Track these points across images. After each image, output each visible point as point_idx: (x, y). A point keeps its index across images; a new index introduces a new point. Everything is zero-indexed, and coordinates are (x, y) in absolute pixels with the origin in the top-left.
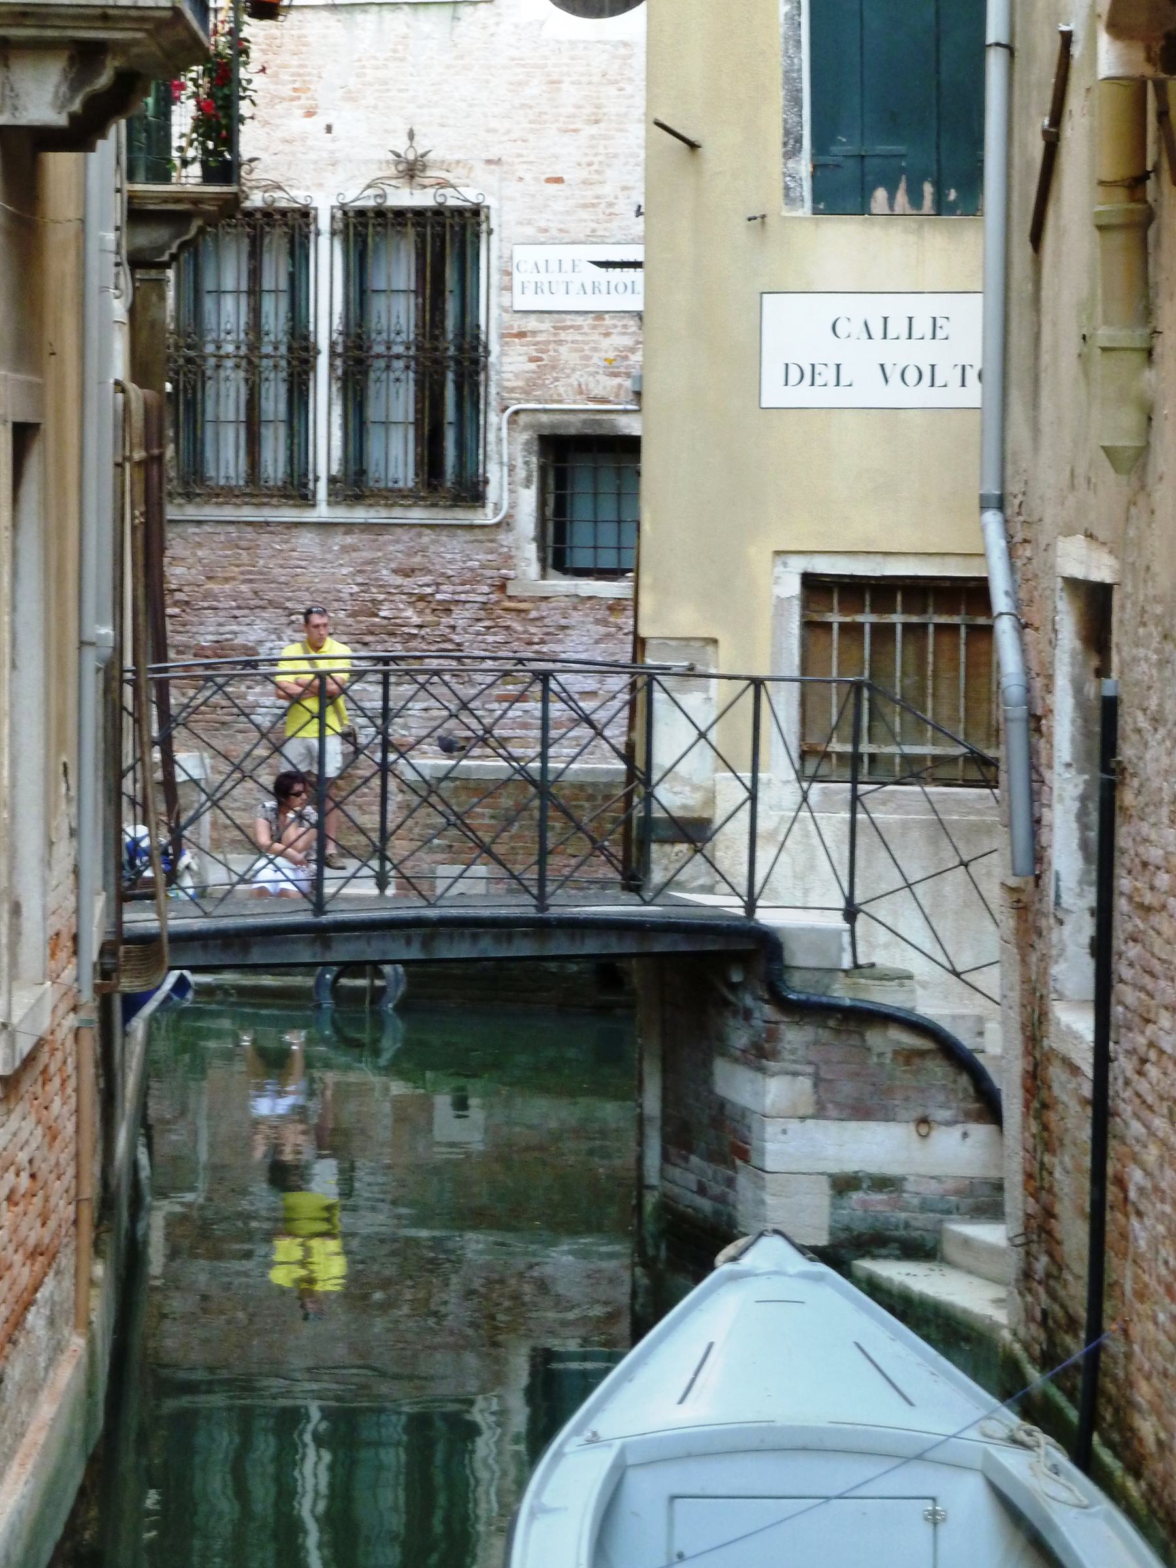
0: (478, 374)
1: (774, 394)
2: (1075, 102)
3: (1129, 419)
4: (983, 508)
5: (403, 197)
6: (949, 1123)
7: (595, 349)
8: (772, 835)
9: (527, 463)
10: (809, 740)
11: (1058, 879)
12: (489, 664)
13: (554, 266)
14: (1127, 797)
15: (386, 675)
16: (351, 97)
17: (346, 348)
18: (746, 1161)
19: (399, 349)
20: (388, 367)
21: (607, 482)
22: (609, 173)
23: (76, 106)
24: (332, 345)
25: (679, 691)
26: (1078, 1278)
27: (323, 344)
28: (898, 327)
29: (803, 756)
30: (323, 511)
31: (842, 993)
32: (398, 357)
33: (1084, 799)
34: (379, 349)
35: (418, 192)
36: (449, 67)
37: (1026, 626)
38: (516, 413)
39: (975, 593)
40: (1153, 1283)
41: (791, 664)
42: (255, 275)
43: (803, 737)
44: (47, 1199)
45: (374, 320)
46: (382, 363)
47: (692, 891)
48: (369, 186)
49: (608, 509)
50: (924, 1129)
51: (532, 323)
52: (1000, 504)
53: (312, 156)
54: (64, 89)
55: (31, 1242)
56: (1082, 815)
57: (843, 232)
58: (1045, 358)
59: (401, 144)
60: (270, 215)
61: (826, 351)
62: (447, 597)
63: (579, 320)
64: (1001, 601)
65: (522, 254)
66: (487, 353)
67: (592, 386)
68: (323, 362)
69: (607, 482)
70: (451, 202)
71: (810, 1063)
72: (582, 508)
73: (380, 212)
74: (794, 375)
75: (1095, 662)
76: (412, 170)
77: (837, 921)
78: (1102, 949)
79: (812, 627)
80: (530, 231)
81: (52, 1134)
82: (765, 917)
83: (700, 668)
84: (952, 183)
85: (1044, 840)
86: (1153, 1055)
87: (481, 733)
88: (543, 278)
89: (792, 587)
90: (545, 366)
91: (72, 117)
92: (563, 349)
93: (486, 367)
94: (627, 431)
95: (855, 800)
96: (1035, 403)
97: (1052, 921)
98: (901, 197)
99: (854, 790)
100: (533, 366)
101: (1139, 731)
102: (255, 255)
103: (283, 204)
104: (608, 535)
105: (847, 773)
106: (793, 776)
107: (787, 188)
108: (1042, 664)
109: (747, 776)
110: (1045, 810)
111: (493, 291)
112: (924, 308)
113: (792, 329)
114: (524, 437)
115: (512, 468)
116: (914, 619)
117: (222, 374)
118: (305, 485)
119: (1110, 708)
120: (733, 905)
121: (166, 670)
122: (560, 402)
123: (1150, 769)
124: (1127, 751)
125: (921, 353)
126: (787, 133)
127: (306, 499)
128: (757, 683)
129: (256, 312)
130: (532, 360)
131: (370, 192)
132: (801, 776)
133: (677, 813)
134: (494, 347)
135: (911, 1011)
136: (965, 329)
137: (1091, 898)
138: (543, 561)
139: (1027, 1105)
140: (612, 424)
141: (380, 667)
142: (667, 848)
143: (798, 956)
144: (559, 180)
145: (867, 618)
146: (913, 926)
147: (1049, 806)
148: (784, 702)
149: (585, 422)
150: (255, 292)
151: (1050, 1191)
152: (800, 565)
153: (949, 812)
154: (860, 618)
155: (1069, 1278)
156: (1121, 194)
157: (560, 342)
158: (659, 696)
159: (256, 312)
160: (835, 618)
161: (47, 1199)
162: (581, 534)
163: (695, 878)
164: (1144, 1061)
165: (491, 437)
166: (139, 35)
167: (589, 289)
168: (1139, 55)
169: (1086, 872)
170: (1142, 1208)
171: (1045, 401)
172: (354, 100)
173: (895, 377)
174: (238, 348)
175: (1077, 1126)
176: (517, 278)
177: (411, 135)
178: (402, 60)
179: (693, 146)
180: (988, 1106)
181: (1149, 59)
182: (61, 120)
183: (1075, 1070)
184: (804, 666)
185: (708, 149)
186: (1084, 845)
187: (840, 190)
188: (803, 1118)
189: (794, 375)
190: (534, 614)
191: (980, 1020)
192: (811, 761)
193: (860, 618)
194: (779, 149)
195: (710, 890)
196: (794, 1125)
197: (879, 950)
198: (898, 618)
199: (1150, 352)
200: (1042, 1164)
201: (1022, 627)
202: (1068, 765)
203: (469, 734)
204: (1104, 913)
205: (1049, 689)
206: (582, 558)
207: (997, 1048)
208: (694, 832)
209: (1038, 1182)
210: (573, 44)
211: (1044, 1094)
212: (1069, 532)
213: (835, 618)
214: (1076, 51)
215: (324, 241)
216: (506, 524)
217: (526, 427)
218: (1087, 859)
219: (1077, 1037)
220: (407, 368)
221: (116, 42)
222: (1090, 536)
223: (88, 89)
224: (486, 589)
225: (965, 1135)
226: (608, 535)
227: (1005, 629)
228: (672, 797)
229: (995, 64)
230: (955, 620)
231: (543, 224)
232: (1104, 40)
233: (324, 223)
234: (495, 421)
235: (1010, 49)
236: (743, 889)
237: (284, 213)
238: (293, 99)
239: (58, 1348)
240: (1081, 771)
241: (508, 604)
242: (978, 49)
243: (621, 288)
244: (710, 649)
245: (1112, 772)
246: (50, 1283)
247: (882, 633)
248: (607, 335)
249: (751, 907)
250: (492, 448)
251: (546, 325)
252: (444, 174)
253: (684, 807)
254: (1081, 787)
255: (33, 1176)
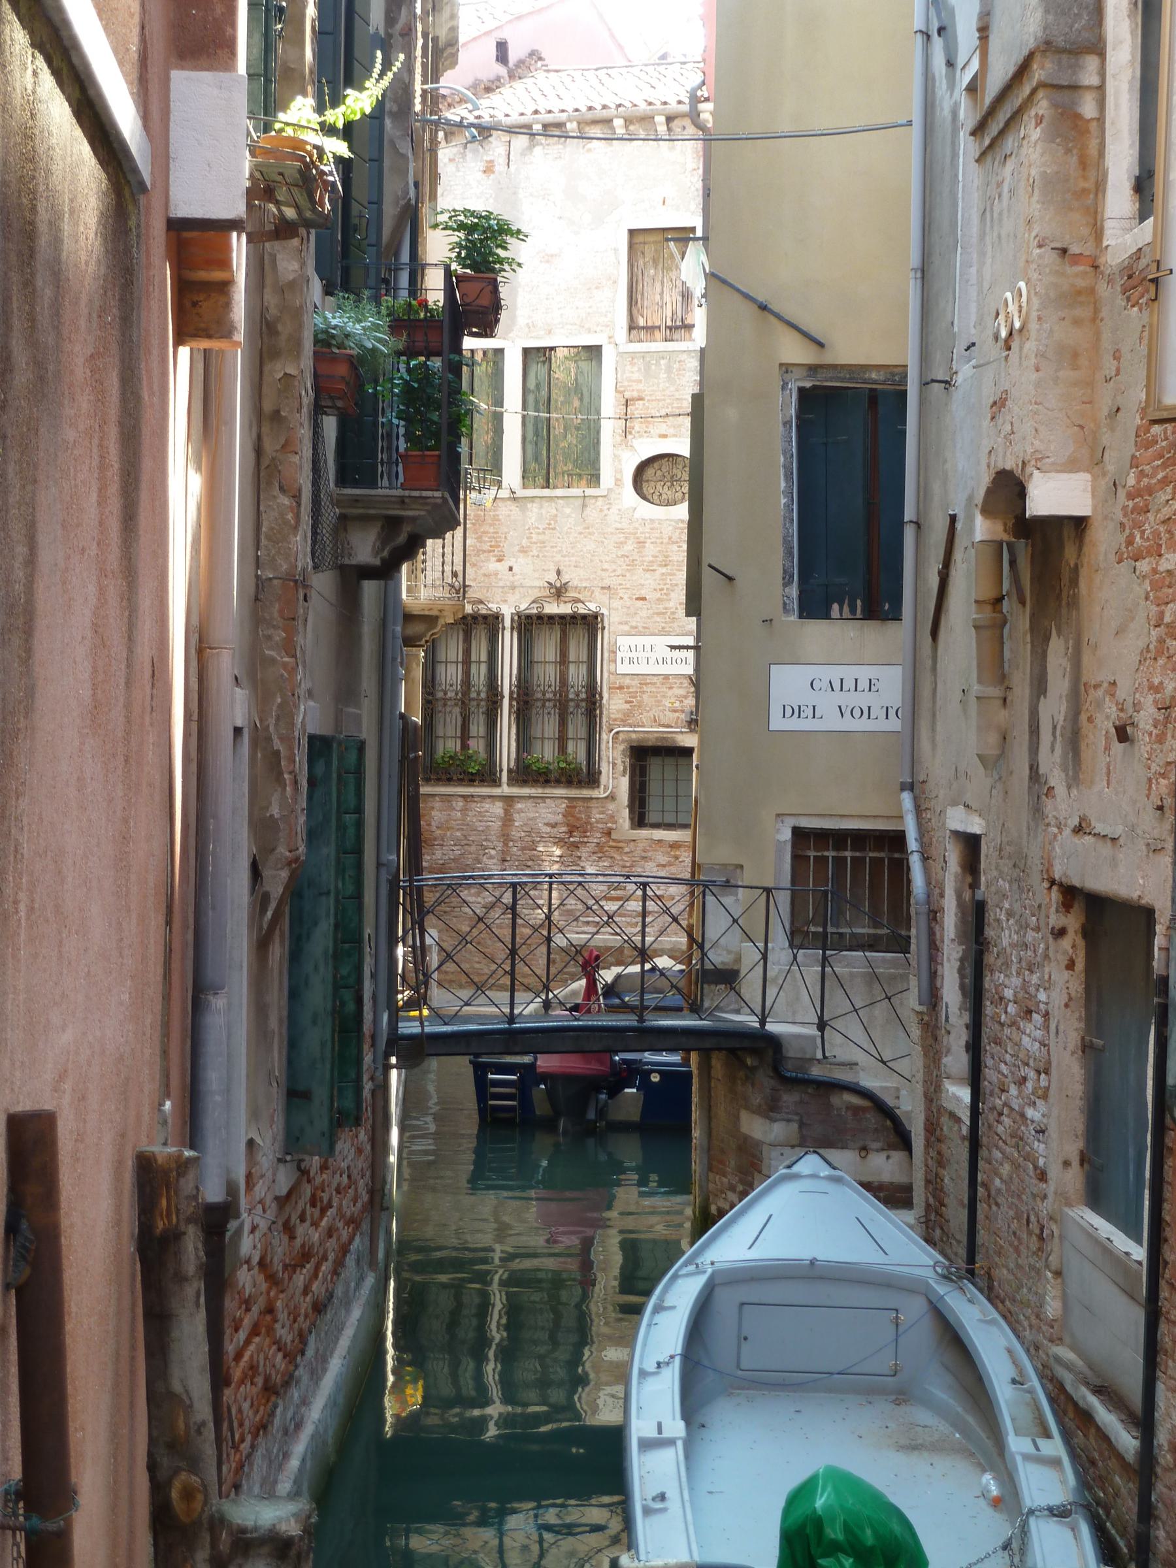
0: (595, 710)
1: (777, 723)
2: (958, 555)
3: (993, 738)
4: (902, 790)
5: (552, 608)
6: (877, 1151)
7: (664, 696)
8: (775, 979)
9: (624, 762)
10: (796, 924)
11: (947, 1007)
12: (601, 879)
13: (640, 648)
14: (989, 959)
15: (551, 884)
16: (524, 551)
17: (518, 695)
18: (760, 1172)
19: (549, 696)
20: (544, 706)
21: (669, 773)
22: (673, 595)
23: (385, 553)
24: (511, 693)
25: (723, 896)
26: (959, 1242)
27: (506, 693)
28: (849, 684)
29: (792, 933)
30: (505, 789)
31: (816, 1072)
32: (549, 700)
33: (962, 960)
34: (539, 695)
35: (562, 605)
36: (581, 533)
37: (928, 858)
38: (617, 733)
39: (897, 840)
40: (1006, 1246)
41: (786, 880)
42: (467, 652)
43: (792, 923)
44: (356, 1190)
45: (536, 679)
46: (475, 703)
47: (726, 1012)
48: (533, 602)
49: (669, 789)
50: (863, 1154)
51: (627, 681)
52: (911, 787)
53: (501, 584)
54: (378, 543)
55: (348, 1214)
56: (961, 970)
57: (816, 629)
58: (939, 703)
59: (552, 577)
60: (476, 618)
61: (807, 698)
62: (577, 839)
63: (655, 679)
64: (912, 844)
65: (623, 641)
66: (601, 698)
67: (662, 717)
68: (506, 702)
69: (669, 773)
70: (582, 611)
71: (797, 1114)
72: (654, 788)
73: (540, 617)
74: (789, 711)
75: (969, 879)
76: (559, 592)
77: (813, 1031)
78: (975, 1048)
79: (798, 859)
80: (626, 628)
81: (359, 1151)
82: (770, 1027)
83: (733, 882)
84: (878, 600)
85: (938, 985)
86: (1006, 1111)
87: (605, 919)
88: (634, 655)
89: (787, 835)
90: (634, 705)
91: (383, 560)
92: (645, 697)
93: (601, 706)
94: (682, 744)
95: (825, 961)
96: (933, 730)
97: (943, 1031)
98: (846, 608)
99: (824, 953)
100: (628, 706)
101: (998, 920)
102: (467, 640)
103: (484, 612)
104: (670, 804)
105: (819, 944)
106: (787, 944)
107: (785, 604)
108: (937, 881)
109: (761, 945)
110: (939, 967)
111: (605, 663)
112: (864, 673)
113: (789, 685)
114: (622, 747)
115: (614, 764)
116: (858, 854)
117: (448, 709)
118: (495, 774)
119: (980, 908)
120: (753, 1022)
121: (422, 880)
122: (643, 726)
123: (1005, 942)
124: (990, 932)
125: (862, 700)
126: (785, 572)
127: (496, 782)
128: (768, 891)
129: (467, 673)
130: (627, 702)
131: (535, 605)
132: (791, 946)
133: (719, 967)
134: (605, 695)
135: (857, 1084)
136: (890, 685)
137: (967, 1018)
138: (631, 819)
139: (927, 1140)
140: (673, 740)
141: (547, 879)
142: (713, 987)
143: (791, 1052)
144: (644, 599)
145: (830, 854)
146: (858, 1035)
147: (942, 964)
148: (783, 899)
149: (657, 739)
150: (467, 662)
151: (942, 1190)
152: (791, 822)
153: (878, 967)
154: (826, 854)
155: (954, 1242)
156: (989, 608)
157: (644, 692)
158: (710, 899)
159: (467, 673)
160: (812, 854)
161: (356, 1190)
162: (653, 804)
163: (728, 1005)
164: (1001, 1114)
165: (603, 747)
166: (422, 513)
167: (660, 661)
168: (999, 527)
169: (964, 1003)
170: (999, 1201)
171: (939, 728)
172: (526, 552)
173: (847, 714)
174: (456, 694)
175: (959, 1153)
176: (619, 655)
177: (559, 573)
178: (554, 529)
179: (730, 579)
180: (903, 1141)
181: (1005, 531)
182: (378, 562)
183: (958, 1120)
184: (794, 881)
185: (739, 582)
186: (962, 987)
187: (813, 606)
188: (793, 1147)
189: (789, 711)
190: (627, 850)
191: (898, 1089)
192: (798, 938)
193: (826, 854)
194: (780, 581)
195: (738, 1012)
196: (787, 1150)
197: (838, 1048)
198: (848, 854)
199: (1005, 700)
200: (937, 1175)
201: (925, 859)
202: (953, 940)
203: (597, 919)
204: (976, 1027)
205: (942, 895)
206: (652, 817)
207: (910, 1107)
208: (728, 977)
209: (934, 1183)
210: (652, 521)
211: (938, 1132)
212: (955, 804)
213: (812, 854)
214: (959, 526)
215: (507, 633)
216: (612, 797)
217: (623, 741)
218: (964, 994)
219: (958, 1099)
220: (555, 706)
221: (408, 517)
222: (967, 806)
223: (393, 544)
224: (598, 835)
225: (888, 1157)
226: (670, 804)
227: (915, 861)
228: (718, 958)
229: (909, 534)
230: (882, 855)
231: (634, 624)
232: (979, 520)
233: (508, 623)
234: (606, 737)
235: (918, 525)
236: (758, 1010)
237: (485, 617)
238: (490, 551)
239: (362, 1278)
240: (960, 944)
241: (611, 843)
242: (900, 524)
243: (679, 661)
244: (738, 871)
245: (982, 944)
246: (357, 1240)
247: (840, 862)
248: (671, 688)
249: (763, 1022)
250: (603, 753)
251: (636, 682)
252: (576, 595)
253: (723, 963)
254: (960, 954)
255: (349, 1177)
